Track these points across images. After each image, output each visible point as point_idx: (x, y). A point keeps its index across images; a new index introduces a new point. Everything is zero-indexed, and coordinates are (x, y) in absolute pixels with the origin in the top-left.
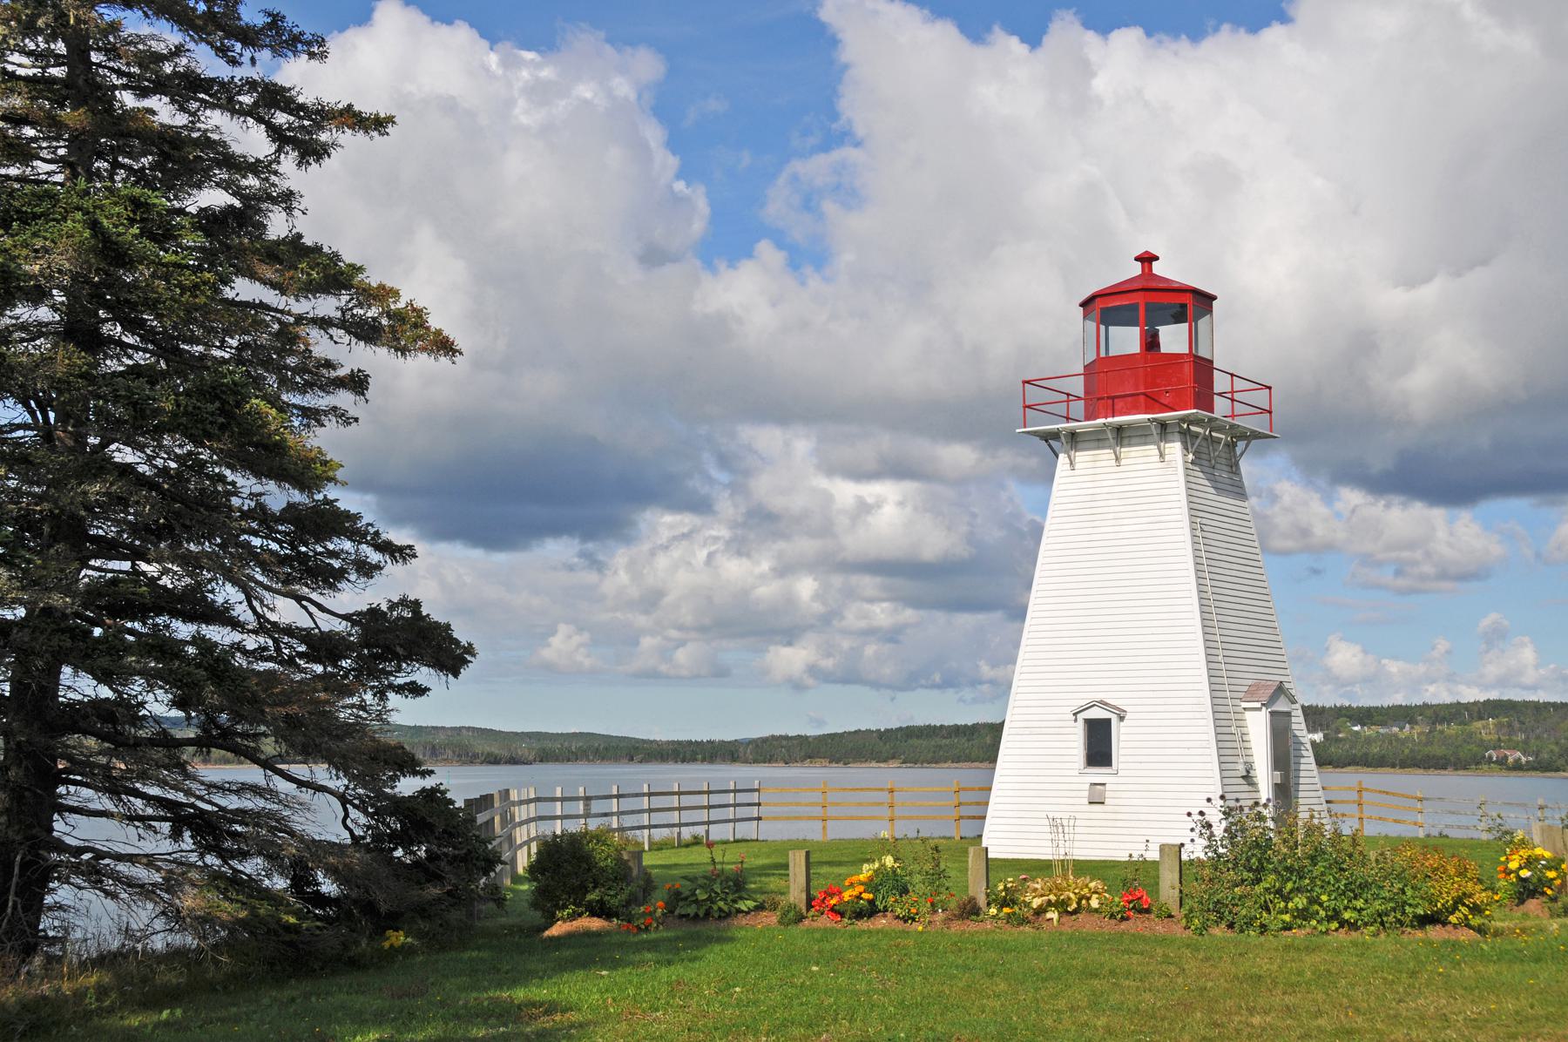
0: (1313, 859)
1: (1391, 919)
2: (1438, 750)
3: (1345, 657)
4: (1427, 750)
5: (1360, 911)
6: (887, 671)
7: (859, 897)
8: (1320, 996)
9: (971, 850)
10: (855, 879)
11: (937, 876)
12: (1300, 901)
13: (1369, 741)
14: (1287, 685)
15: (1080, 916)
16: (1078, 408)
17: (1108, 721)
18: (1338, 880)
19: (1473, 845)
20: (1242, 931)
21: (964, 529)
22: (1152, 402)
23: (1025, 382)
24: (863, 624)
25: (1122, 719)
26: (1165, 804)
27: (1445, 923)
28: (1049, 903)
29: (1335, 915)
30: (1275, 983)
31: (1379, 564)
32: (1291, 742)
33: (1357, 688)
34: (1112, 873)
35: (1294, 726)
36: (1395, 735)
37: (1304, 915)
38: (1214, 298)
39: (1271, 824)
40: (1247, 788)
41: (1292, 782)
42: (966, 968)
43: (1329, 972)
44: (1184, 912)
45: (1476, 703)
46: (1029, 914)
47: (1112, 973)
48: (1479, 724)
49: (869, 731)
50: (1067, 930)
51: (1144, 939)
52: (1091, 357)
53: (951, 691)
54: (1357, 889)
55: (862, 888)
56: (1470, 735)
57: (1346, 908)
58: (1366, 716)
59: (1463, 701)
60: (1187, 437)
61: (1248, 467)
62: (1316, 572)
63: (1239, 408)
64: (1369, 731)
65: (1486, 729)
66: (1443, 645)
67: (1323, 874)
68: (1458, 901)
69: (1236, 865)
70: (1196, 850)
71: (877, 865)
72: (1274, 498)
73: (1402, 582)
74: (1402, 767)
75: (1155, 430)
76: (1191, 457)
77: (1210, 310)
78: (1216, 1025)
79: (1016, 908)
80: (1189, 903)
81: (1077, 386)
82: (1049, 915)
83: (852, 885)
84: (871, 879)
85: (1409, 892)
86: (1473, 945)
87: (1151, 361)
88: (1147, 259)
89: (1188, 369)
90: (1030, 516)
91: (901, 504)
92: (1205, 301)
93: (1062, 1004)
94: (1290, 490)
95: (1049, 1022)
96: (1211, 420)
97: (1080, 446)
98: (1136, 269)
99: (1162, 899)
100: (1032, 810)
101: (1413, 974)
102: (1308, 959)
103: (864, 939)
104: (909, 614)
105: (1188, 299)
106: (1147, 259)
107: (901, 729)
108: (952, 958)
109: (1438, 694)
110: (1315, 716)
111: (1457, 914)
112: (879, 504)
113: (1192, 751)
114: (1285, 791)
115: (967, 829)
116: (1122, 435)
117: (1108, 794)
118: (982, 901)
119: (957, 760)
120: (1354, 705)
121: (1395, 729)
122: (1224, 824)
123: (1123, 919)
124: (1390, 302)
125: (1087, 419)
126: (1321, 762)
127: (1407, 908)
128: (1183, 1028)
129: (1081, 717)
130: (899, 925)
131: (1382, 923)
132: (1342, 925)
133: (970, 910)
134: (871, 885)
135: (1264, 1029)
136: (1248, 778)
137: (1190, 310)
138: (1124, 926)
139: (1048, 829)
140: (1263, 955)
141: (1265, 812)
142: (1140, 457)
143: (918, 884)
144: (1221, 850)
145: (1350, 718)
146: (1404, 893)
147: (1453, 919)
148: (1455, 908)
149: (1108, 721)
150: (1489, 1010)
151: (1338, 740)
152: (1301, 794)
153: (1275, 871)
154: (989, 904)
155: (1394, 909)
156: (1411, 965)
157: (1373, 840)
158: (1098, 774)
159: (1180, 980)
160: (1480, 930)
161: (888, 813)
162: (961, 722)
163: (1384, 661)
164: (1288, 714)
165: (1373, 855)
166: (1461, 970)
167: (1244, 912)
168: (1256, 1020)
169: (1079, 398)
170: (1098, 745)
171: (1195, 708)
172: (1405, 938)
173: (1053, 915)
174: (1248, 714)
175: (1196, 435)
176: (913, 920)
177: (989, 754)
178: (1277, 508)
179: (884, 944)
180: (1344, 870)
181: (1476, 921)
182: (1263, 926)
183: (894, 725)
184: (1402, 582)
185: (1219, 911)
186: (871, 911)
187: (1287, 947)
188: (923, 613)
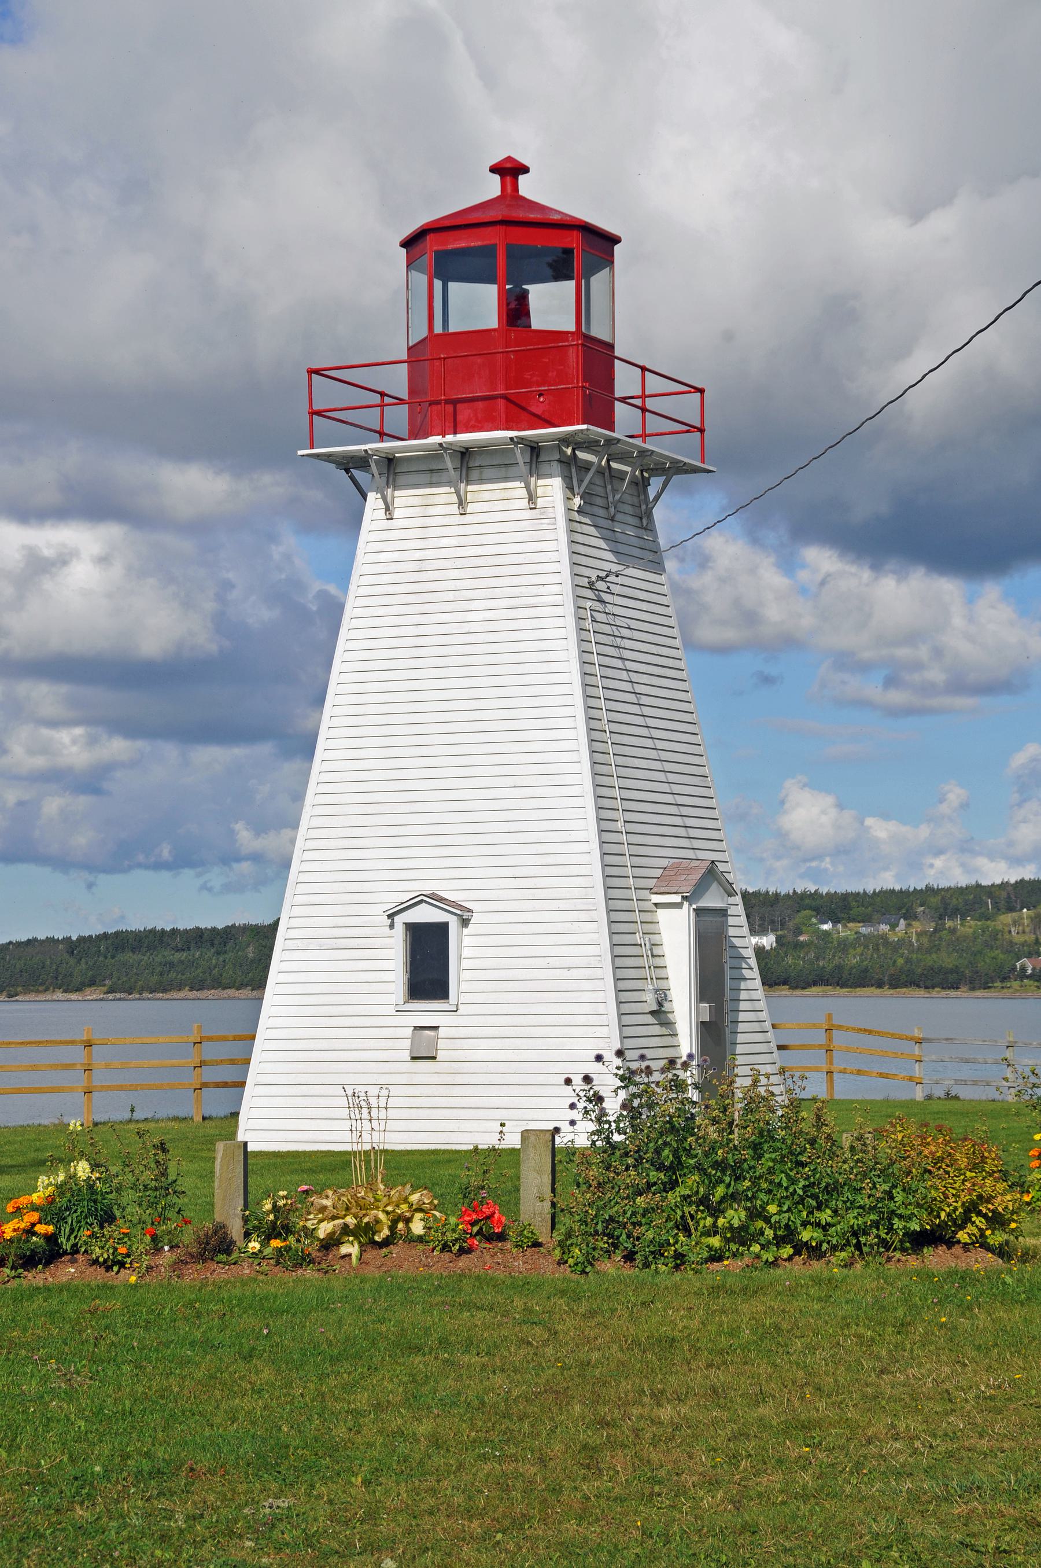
0: (756, 1148)
1: (872, 1239)
2: (947, 960)
3: (809, 814)
4: (931, 959)
5: (825, 1227)
6: (82, 840)
7: (30, 1232)
8: (764, 1369)
9: (220, 1146)
10: (23, 1200)
11: (162, 1190)
12: (735, 1216)
13: (844, 946)
14: (721, 867)
15: (394, 1249)
16: (398, 417)
17: (444, 927)
18: (793, 1181)
19: (994, 1111)
20: (646, 1265)
21: (210, 606)
22: (517, 413)
23: (311, 372)
24: (39, 762)
25: (465, 922)
26: (530, 1062)
27: (950, 1243)
28: (346, 1230)
29: (787, 1236)
30: (696, 1351)
31: (864, 668)
32: (726, 956)
33: (827, 863)
34: (445, 1172)
35: (731, 932)
36: (884, 937)
37: (741, 1236)
38: (615, 240)
39: (693, 1095)
40: (657, 1030)
41: (728, 1018)
42: (208, 1345)
43: (777, 1328)
44: (557, 1237)
45: (1004, 885)
46: (313, 1250)
47: (444, 1343)
48: (1007, 918)
49: (51, 941)
50: (373, 1272)
51: (495, 1285)
52: (421, 332)
53: (188, 873)
54: (821, 1194)
55: (35, 1216)
56: (995, 935)
57: (804, 1224)
58: (840, 907)
59: (985, 882)
60: (572, 470)
61: (671, 513)
62: (767, 680)
63: (654, 424)
64: (845, 931)
65: (1017, 925)
66: (955, 794)
67: (771, 1171)
68: (971, 1208)
69: (639, 1161)
70: (580, 1135)
71: (61, 1177)
72: (704, 562)
73: (897, 697)
74: (894, 986)
75: (521, 456)
76: (577, 501)
77: (608, 260)
78: (604, 1423)
79: (292, 1239)
80: (566, 1221)
81: (397, 381)
82: (344, 1249)
83: (18, 1211)
84: (51, 1200)
85: (899, 1197)
86: (993, 1276)
87: (513, 343)
88: (510, 171)
89: (573, 357)
90: (317, 586)
91: (103, 560)
92: (601, 244)
93: (362, 1399)
94: (727, 548)
95: (340, 1432)
96: (610, 441)
97: (402, 479)
98: (493, 187)
99: (525, 1217)
100: (320, 1072)
101: (902, 1327)
102: (747, 1308)
103: (38, 1303)
104: (118, 747)
105: (574, 240)
106: (510, 171)
107: (105, 936)
108: (184, 1328)
109: (948, 873)
110: (763, 909)
111: (970, 1228)
112: (64, 559)
113: (575, 973)
114: (715, 1034)
115: (215, 1104)
116: (468, 464)
117: (441, 1044)
118: (236, 1230)
119: (198, 985)
120: (824, 890)
121: (884, 928)
122: (623, 1094)
123: (462, 1251)
124: (881, 240)
125: (414, 435)
126: (769, 981)
127: (896, 1221)
128: (553, 1431)
129: (400, 920)
130: (99, 1276)
131: (858, 1246)
132: (797, 1252)
133: (217, 1246)
134: (50, 1211)
135: (677, 1427)
136: (660, 1014)
137: (578, 260)
138: (463, 1262)
139: (343, 1102)
140: (679, 1302)
141: (683, 1075)
142: (499, 500)
143: (131, 1207)
144: (617, 1138)
145: (817, 910)
146: (891, 1198)
147: (962, 1236)
148: (966, 1220)
149: (444, 927)
150: (1013, 1383)
151: (798, 946)
152: (739, 1049)
153: (699, 1168)
154: (247, 1235)
155: (876, 1224)
156: (900, 1312)
157: (845, 1106)
158: (426, 1013)
159: (549, 1351)
160: (1003, 1252)
161: (81, 1080)
162: (205, 924)
163: (869, 821)
164: (723, 913)
165: (846, 1140)
166: (973, 1317)
167: (650, 1235)
168: (666, 1413)
169: (401, 401)
170: (428, 965)
171: (580, 904)
172: (892, 1268)
173: (350, 1248)
174: (662, 914)
175: (586, 467)
176: (122, 1265)
177: (254, 975)
178: (707, 578)
179: (72, 1310)
180: (803, 1165)
181: (996, 1238)
182: (679, 1256)
183: (94, 928)
184: (897, 697)
185: (613, 1235)
186: (51, 1253)
187: (715, 1290)
188: (140, 744)
